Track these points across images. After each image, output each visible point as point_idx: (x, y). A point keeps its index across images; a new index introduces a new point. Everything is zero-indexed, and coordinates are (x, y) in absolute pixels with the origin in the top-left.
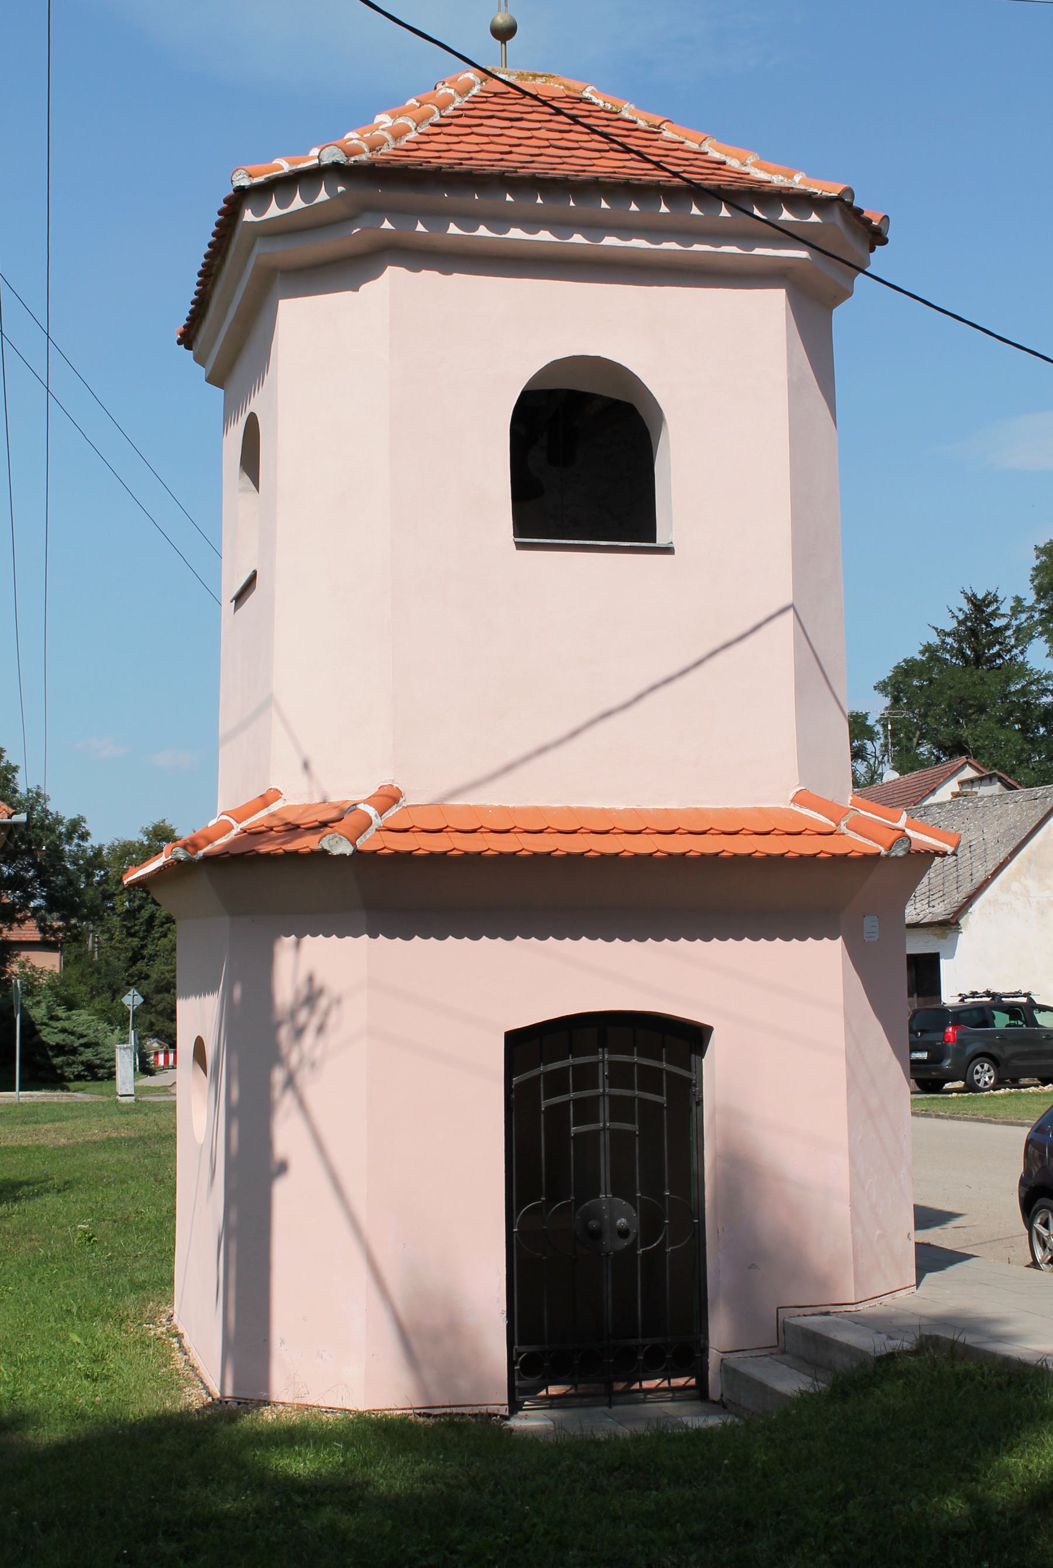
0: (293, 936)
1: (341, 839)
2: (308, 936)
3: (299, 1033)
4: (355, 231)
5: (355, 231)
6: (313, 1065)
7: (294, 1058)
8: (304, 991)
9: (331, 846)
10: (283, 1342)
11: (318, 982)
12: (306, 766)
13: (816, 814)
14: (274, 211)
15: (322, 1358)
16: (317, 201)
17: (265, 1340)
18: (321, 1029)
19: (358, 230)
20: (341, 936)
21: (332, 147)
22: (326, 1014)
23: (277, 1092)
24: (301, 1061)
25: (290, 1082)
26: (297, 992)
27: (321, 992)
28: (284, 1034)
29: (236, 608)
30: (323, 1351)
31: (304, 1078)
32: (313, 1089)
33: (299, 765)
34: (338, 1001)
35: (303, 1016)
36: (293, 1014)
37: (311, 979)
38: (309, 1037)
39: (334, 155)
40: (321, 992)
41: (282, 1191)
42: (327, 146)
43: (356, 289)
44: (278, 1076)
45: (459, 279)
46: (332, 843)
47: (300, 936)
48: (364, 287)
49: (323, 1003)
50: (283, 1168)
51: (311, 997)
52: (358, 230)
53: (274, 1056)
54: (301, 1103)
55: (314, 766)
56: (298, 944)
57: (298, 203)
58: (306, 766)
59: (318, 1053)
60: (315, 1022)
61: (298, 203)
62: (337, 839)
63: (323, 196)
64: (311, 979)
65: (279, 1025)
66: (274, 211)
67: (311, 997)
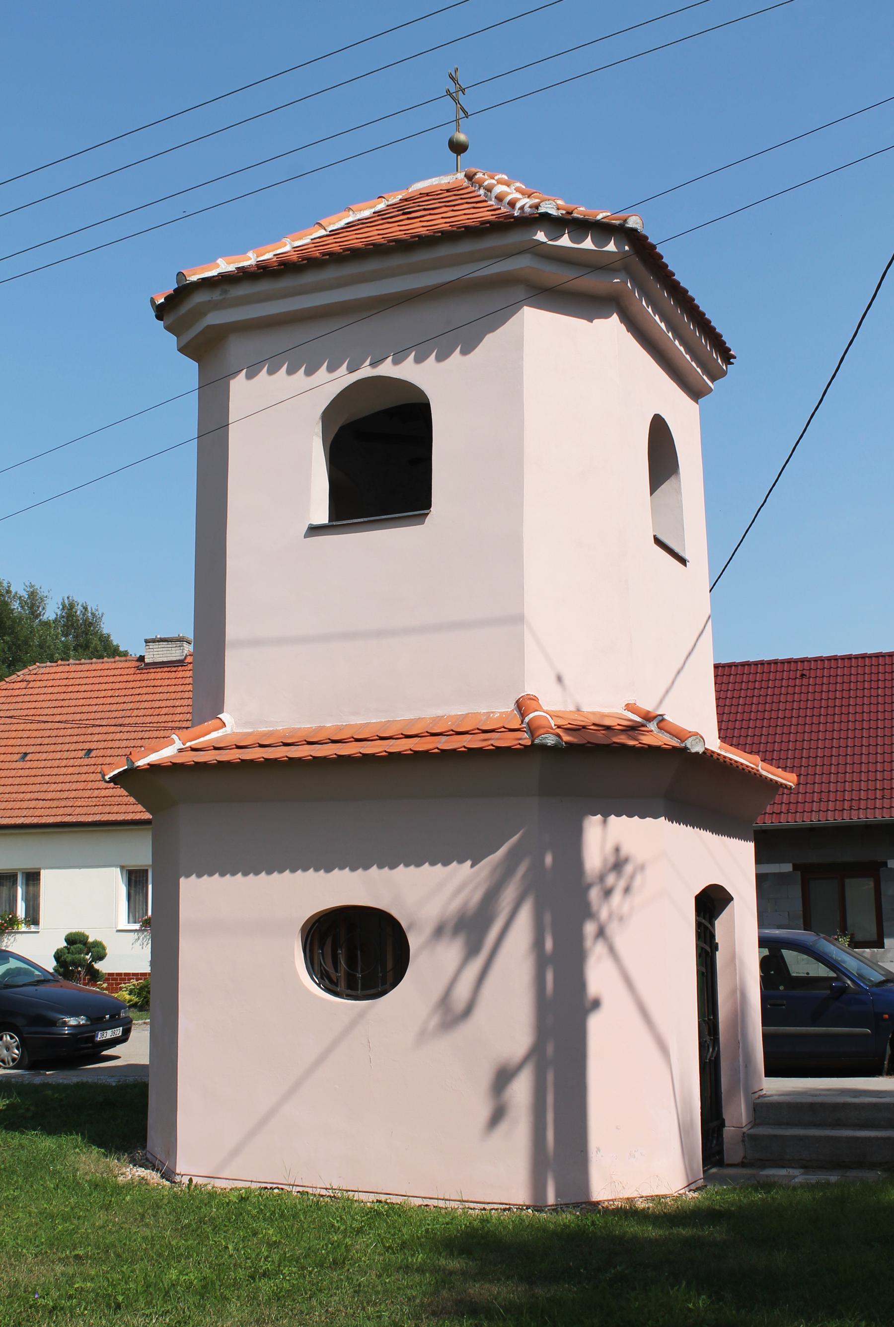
0: (599, 815)
1: (700, 740)
2: (613, 816)
3: (608, 893)
4: (615, 281)
5: (615, 281)
6: (621, 919)
7: (604, 914)
8: (611, 860)
9: (692, 745)
10: (598, 1150)
11: (624, 852)
12: (559, 679)
13: (738, 758)
14: (565, 241)
15: (635, 1157)
16: (605, 249)
17: (582, 1151)
18: (627, 890)
19: (618, 280)
20: (642, 817)
21: (637, 217)
22: (632, 877)
23: (589, 942)
24: (610, 915)
25: (601, 933)
26: (605, 861)
27: (626, 860)
28: (594, 894)
29: (307, 536)
30: (635, 1151)
31: (613, 929)
32: (621, 938)
33: (553, 679)
34: (642, 868)
35: (611, 879)
36: (602, 878)
37: (617, 850)
38: (617, 897)
39: (637, 223)
40: (626, 860)
41: (595, 1024)
42: (635, 215)
43: (591, 320)
44: (590, 929)
45: (629, 337)
46: (694, 742)
47: (606, 816)
48: (596, 321)
49: (629, 869)
50: (596, 1004)
51: (618, 864)
52: (618, 280)
53: (586, 912)
54: (612, 950)
55: (567, 680)
56: (605, 822)
57: (588, 244)
58: (559, 679)
59: (625, 909)
60: (622, 884)
61: (588, 244)
62: (698, 740)
63: (611, 247)
64: (617, 850)
65: (589, 886)
66: (565, 241)
67: (618, 864)
